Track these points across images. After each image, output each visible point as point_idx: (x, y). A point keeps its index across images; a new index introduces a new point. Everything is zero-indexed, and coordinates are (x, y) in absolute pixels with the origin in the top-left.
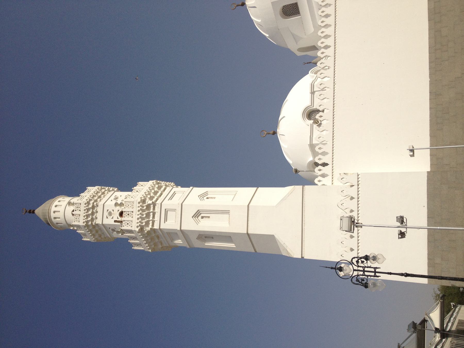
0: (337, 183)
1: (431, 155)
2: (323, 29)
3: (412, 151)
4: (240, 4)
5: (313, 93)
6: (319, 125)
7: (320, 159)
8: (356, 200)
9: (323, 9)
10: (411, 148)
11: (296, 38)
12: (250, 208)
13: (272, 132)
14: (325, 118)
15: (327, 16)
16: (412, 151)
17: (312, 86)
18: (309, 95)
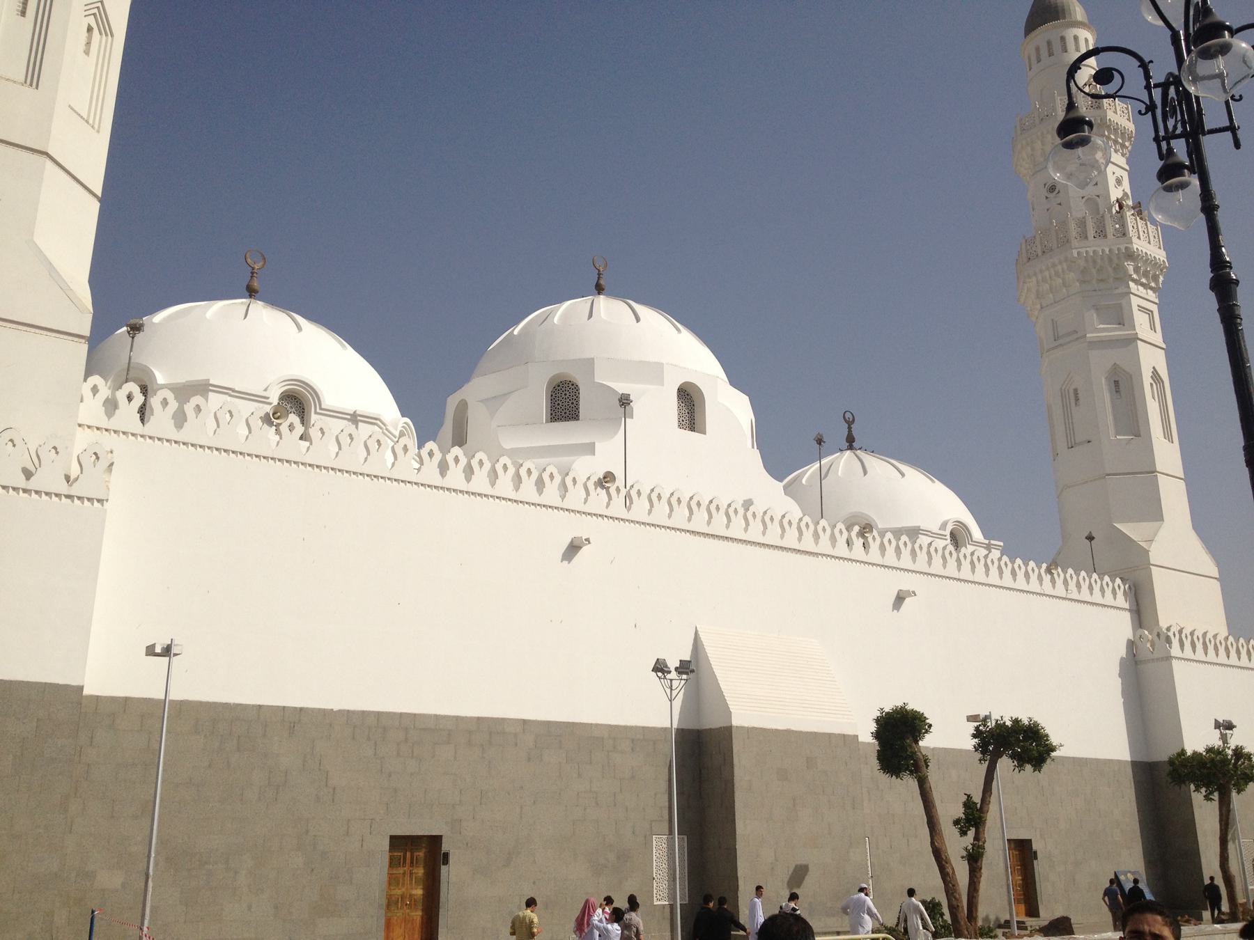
0: (82, 441)
1: (126, 699)
2: (511, 470)
3: (167, 651)
4: (602, 282)
5: (354, 418)
6: (267, 420)
7: (165, 403)
8: (21, 482)
9: (558, 479)
10: (174, 650)
11: (494, 402)
12: (36, 157)
13: (256, 284)
14: (288, 440)
15: (540, 485)
16: (167, 651)
17: (373, 420)
18: (350, 408)
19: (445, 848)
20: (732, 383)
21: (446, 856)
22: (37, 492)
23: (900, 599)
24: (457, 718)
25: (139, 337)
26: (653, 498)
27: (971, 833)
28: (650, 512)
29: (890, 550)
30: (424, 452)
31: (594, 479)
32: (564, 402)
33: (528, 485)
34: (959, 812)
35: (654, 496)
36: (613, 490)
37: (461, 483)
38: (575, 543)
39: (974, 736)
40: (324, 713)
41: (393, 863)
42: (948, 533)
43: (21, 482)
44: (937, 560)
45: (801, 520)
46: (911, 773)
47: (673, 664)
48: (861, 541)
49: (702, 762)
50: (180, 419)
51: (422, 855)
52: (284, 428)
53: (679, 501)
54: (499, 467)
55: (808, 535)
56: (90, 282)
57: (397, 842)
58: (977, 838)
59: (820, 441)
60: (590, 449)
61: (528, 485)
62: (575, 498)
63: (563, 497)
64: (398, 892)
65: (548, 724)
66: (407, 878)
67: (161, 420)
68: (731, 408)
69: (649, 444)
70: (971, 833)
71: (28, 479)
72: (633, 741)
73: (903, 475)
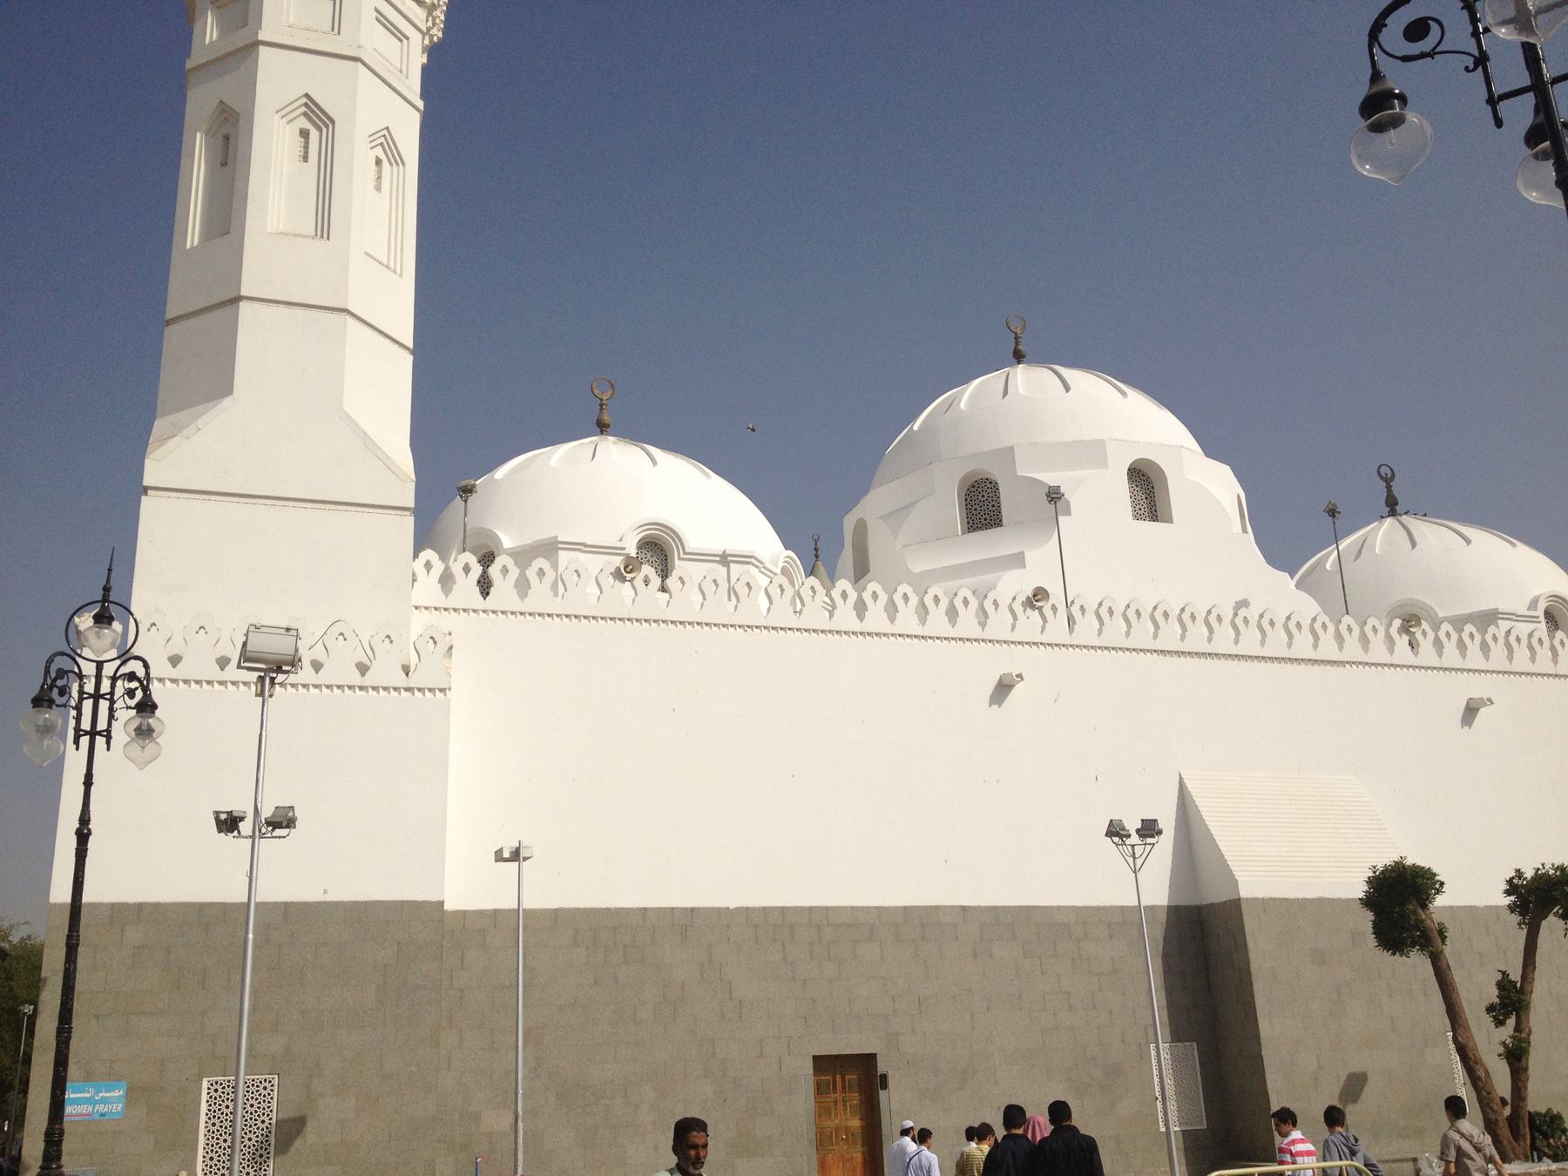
0: (419, 623)
1: (496, 912)
3: (516, 856)
5: (725, 559)
6: (618, 576)
7: (505, 570)
8: (356, 679)
9: (974, 604)
10: (523, 853)
11: (896, 516)
13: (606, 418)
15: (952, 614)
16: (516, 856)
17: (747, 559)
18: (717, 547)
19: (881, 1068)
20: (1209, 453)
21: (884, 1077)
22: (374, 688)
23: (1471, 711)
24: (879, 909)
25: (472, 499)
26: (1102, 614)
27: (1511, 1022)
28: (1100, 632)
29: (1450, 647)
30: (836, 593)
31: (1022, 598)
32: (982, 506)
33: (937, 617)
34: (1493, 995)
35: (1213, 619)
36: (1047, 610)
37: (944, 628)
38: (1005, 682)
39: (1508, 893)
40: (719, 912)
41: (820, 1089)
42: (1540, 613)
43: (356, 679)
44: (1521, 652)
45: (1314, 619)
46: (1423, 948)
47: (1132, 825)
48: (1406, 638)
49: (1204, 950)
50: (523, 586)
51: (853, 1079)
52: (639, 582)
53: (1193, 617)
54: (898, 598)
55: (1327, 639)
56: (412, 445)
57: (823, 1064)
58: (1518, 1029)
59: (1333, 512)
60: (1018, 560)
61: (937, 617)
62: (999, 624)
63: (983, 625)
64: (831, 1123)
65: (995, 910)
66: (840, 1104)
67: (503, 587)
68: (1208, 486)
69: (1097, 542)
70: (1511, 1022)
71: (363, 674)
72: (1109, 925)
73: (1468, 541)
